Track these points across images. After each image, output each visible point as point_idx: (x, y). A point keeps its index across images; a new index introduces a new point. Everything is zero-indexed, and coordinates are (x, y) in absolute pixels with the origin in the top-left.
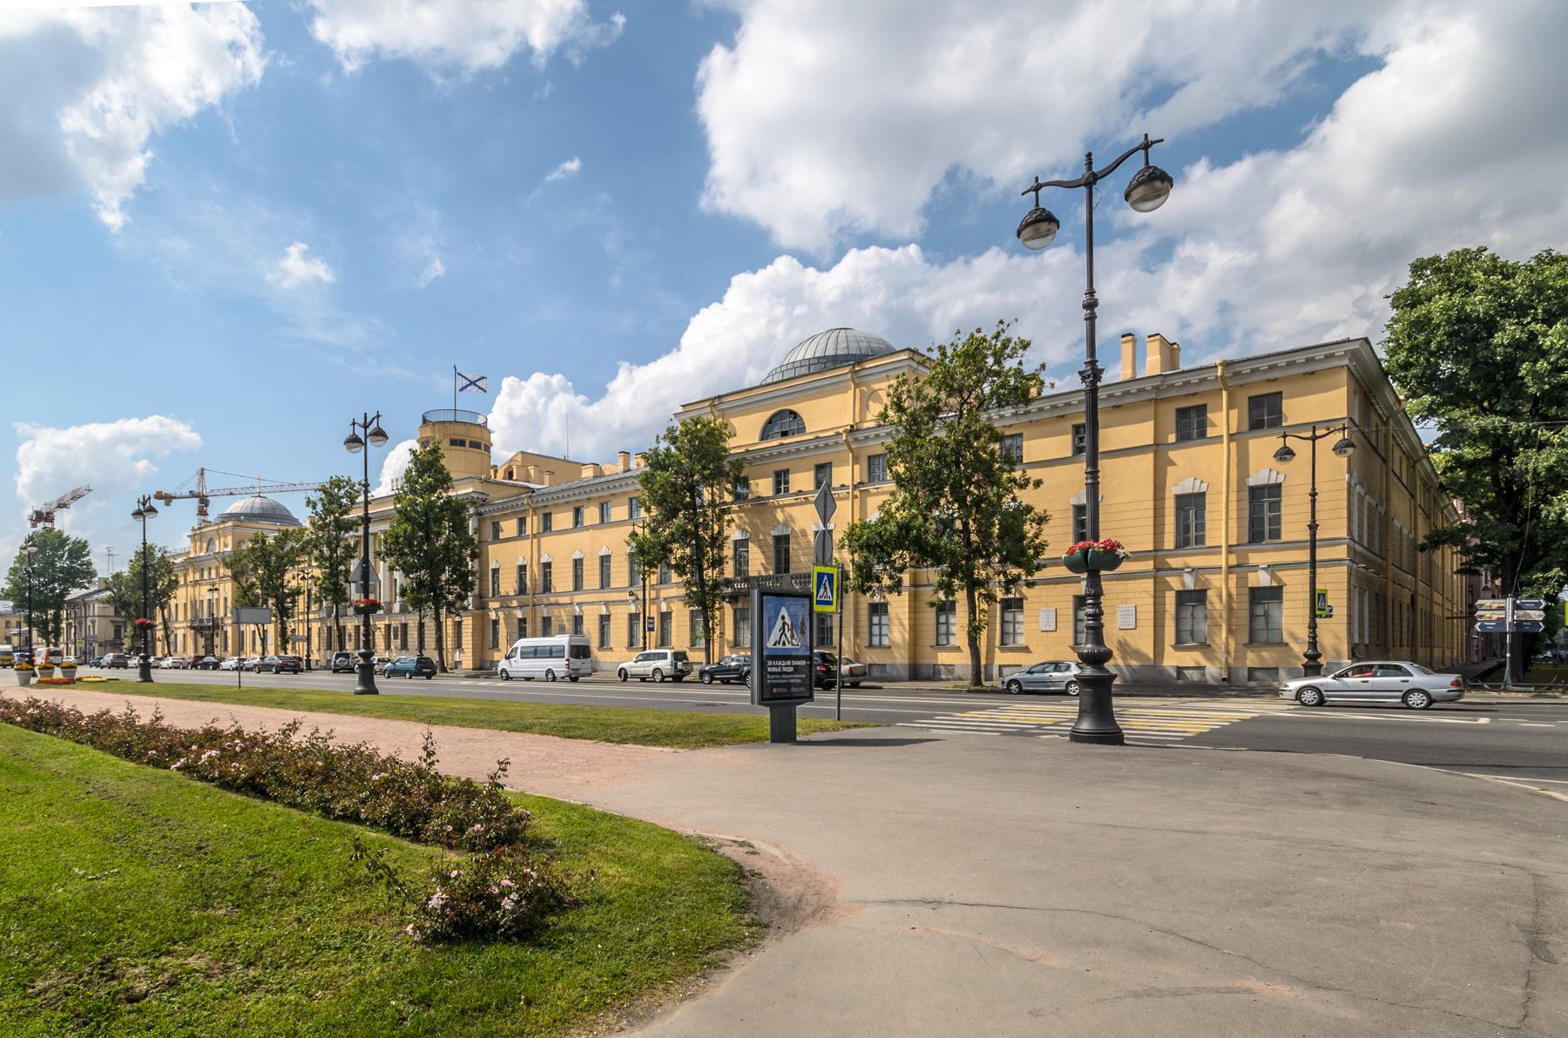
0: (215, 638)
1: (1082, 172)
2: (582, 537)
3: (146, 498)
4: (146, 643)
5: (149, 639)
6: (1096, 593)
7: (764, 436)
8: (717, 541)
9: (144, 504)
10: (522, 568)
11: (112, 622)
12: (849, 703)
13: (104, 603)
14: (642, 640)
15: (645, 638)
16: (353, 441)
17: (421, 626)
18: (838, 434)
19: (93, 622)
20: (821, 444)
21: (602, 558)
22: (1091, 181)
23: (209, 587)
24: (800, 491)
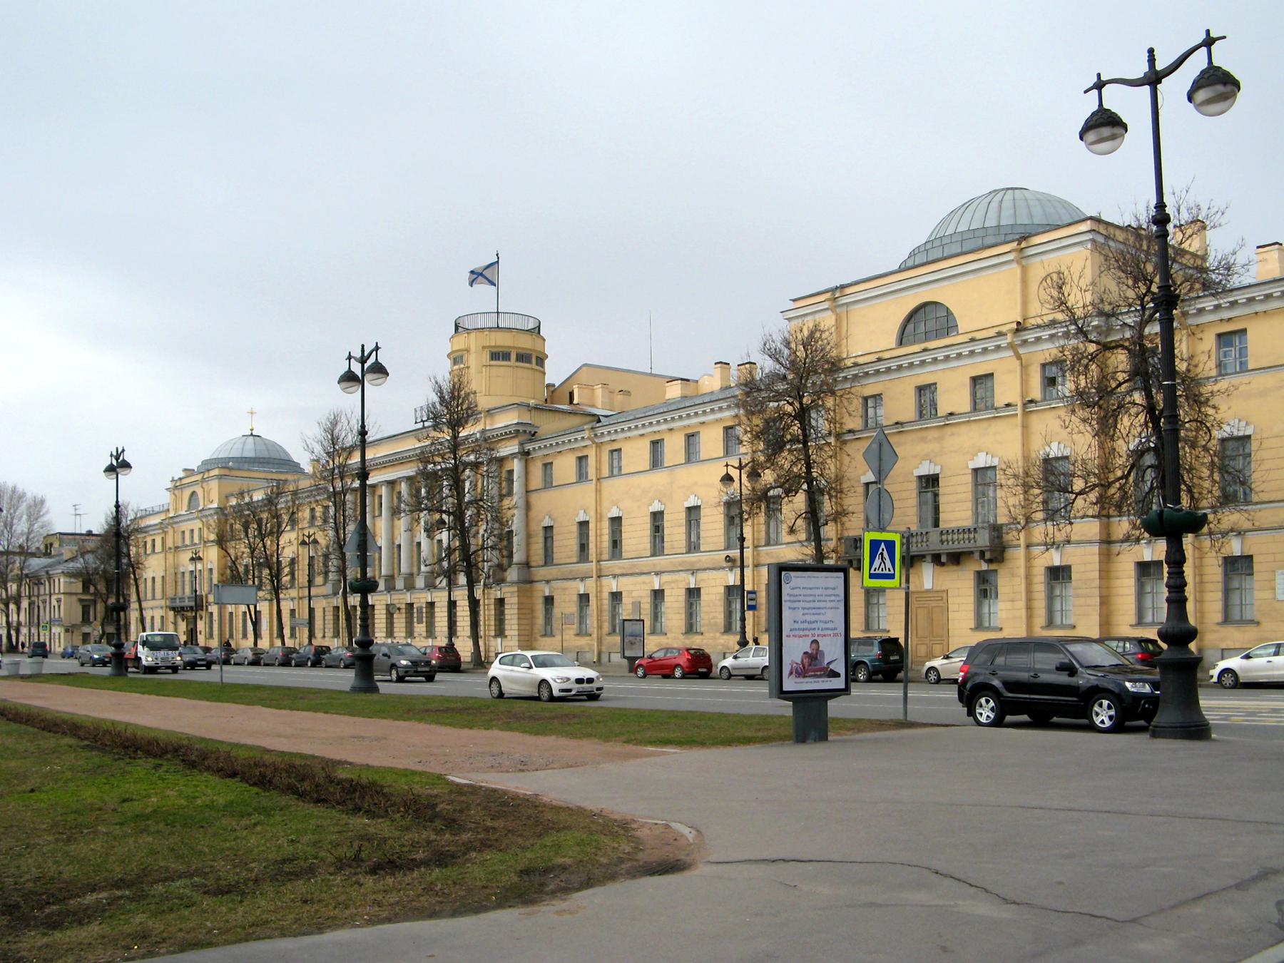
0: (199, 622)
1: (1141, 69)
2: (659, 477)
3: (120, 451)
4: (118, 629)
5: (122, 622)
6: (1176, 559)
7: (901, 343)
8: (837, 488)
9: (117, 459)
10: (584, 525)
11: (81, 600)
12: (919, 700)
13: (70, 577)
14: (739, 623)
15: (743, 619)
16: (349, 377)
17: (452, 605)
18: (1000, 334)
19: (59, 601)
20: (953, 353)
21: (689, 509)
22: (1153, 79)
23: (190, 555)
24: (951, 414)
